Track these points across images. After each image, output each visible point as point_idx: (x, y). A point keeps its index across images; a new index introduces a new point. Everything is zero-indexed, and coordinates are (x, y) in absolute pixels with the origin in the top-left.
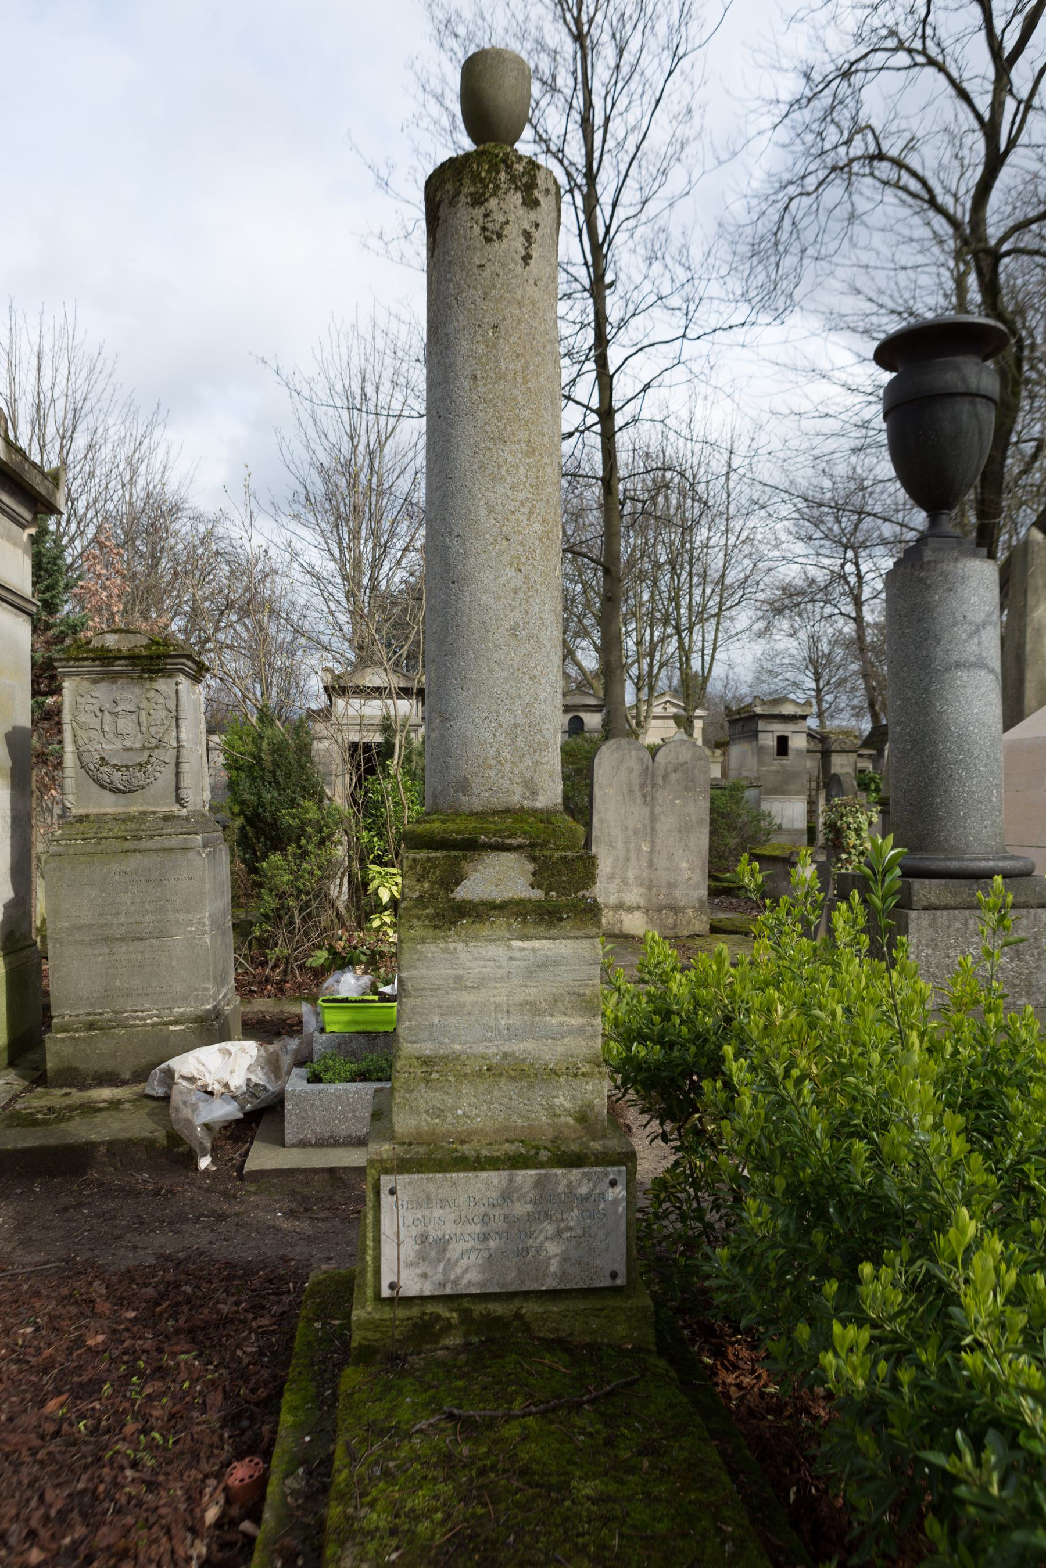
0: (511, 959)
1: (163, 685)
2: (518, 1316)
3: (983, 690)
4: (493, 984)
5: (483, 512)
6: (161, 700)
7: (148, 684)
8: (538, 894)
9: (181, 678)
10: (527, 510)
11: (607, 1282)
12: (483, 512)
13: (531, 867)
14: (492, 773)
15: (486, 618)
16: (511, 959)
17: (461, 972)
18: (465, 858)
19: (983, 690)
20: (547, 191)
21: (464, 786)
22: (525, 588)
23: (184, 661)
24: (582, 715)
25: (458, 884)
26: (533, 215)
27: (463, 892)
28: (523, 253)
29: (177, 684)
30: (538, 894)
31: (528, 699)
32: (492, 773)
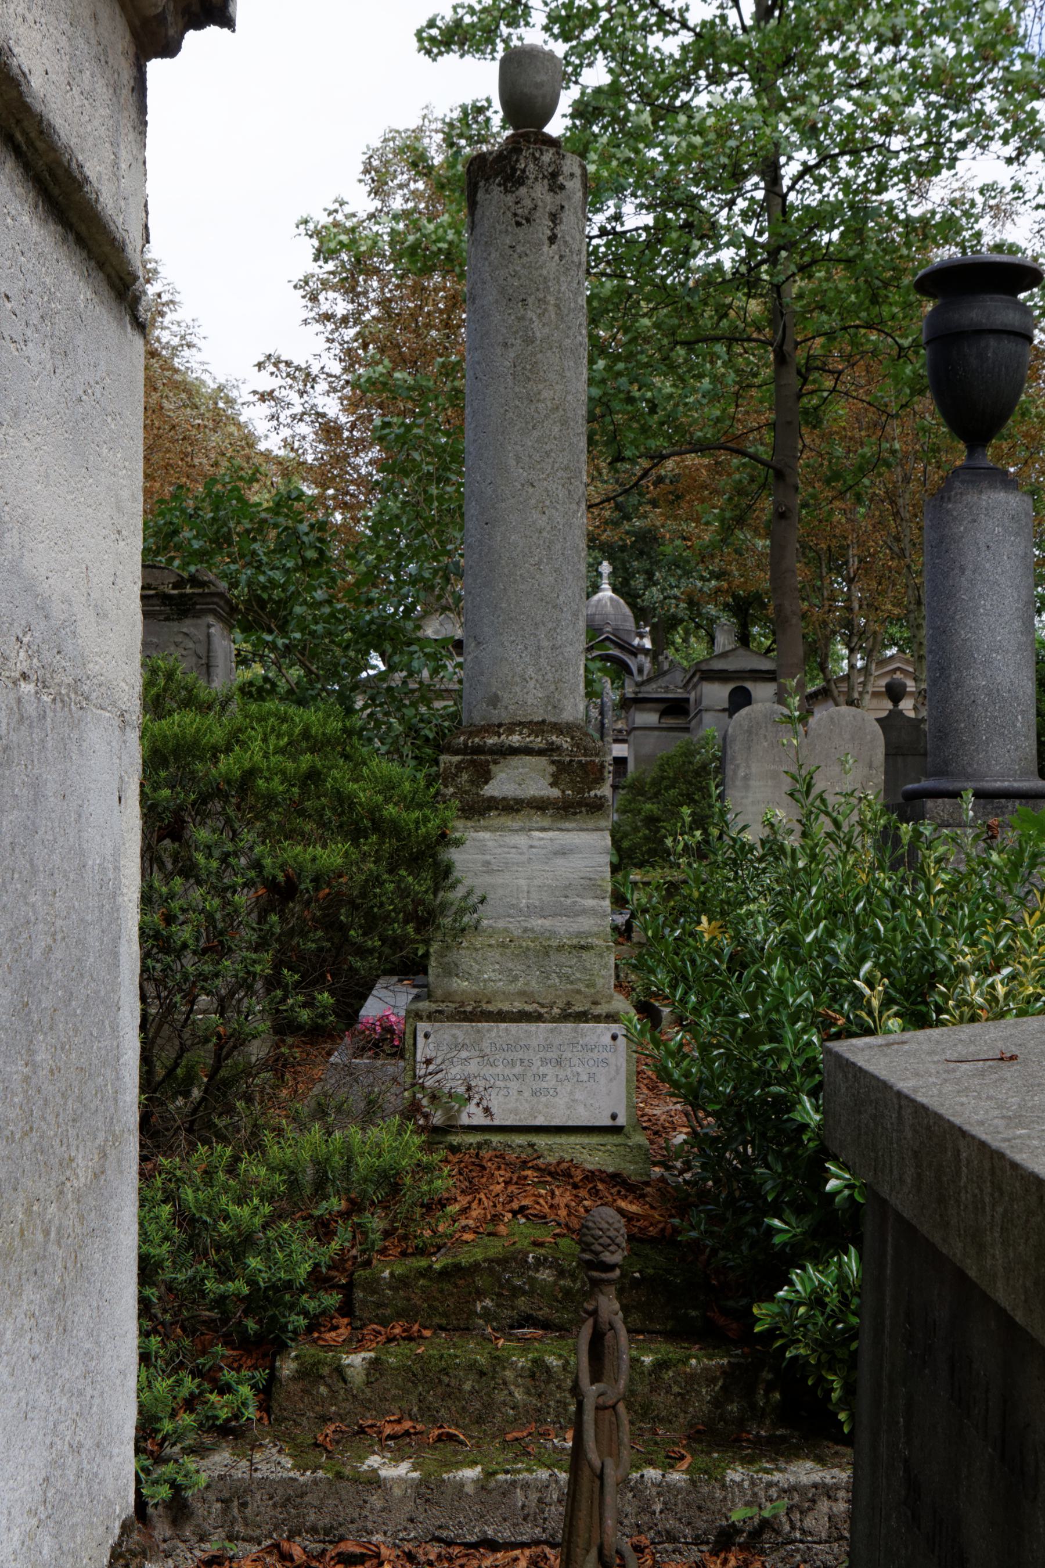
0: (531, 847)
1: (188, 626)
2: (532, 1145)
3: (1007, 618)
4: (515, 868)
5: (512, 462)
6: (191, 645)
7: (175, 626)
8: (555, 793)
9: (211, 619)
10: (551, 460)
11: (608, 1122)
12: (512, 462)
13: (552, 769)
14: (518, 689)
15: (514, 555)
16: (531, 847)
17: (488, 857)
18: (496, 763)
19: (1007, 618)
20: (572, 175)
21: (494, 701)
22: (548, 528)
23: (216, 600)
24: (749, 685)
25: (486, 783)
26: (560, 198)
27: (491, 790)
28: (549, 233)
29: (209, 626)
30: (555, 793)
31: (550, 625)
32: (518, 689)
